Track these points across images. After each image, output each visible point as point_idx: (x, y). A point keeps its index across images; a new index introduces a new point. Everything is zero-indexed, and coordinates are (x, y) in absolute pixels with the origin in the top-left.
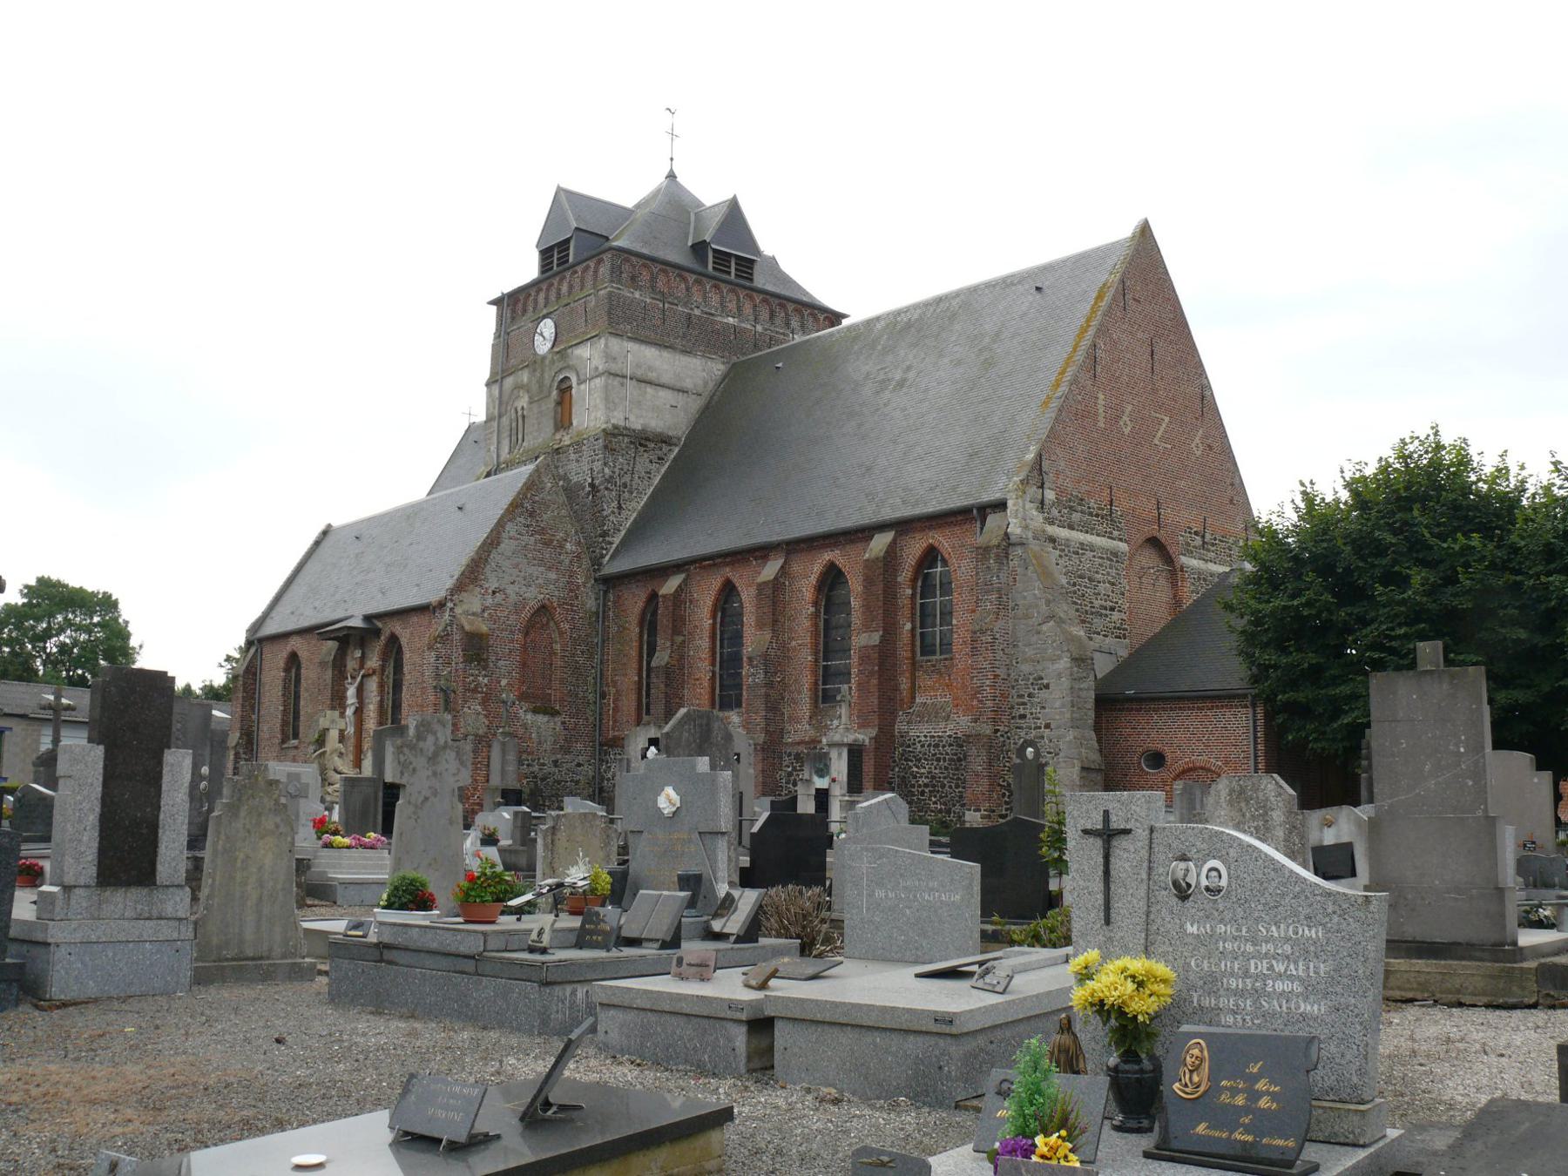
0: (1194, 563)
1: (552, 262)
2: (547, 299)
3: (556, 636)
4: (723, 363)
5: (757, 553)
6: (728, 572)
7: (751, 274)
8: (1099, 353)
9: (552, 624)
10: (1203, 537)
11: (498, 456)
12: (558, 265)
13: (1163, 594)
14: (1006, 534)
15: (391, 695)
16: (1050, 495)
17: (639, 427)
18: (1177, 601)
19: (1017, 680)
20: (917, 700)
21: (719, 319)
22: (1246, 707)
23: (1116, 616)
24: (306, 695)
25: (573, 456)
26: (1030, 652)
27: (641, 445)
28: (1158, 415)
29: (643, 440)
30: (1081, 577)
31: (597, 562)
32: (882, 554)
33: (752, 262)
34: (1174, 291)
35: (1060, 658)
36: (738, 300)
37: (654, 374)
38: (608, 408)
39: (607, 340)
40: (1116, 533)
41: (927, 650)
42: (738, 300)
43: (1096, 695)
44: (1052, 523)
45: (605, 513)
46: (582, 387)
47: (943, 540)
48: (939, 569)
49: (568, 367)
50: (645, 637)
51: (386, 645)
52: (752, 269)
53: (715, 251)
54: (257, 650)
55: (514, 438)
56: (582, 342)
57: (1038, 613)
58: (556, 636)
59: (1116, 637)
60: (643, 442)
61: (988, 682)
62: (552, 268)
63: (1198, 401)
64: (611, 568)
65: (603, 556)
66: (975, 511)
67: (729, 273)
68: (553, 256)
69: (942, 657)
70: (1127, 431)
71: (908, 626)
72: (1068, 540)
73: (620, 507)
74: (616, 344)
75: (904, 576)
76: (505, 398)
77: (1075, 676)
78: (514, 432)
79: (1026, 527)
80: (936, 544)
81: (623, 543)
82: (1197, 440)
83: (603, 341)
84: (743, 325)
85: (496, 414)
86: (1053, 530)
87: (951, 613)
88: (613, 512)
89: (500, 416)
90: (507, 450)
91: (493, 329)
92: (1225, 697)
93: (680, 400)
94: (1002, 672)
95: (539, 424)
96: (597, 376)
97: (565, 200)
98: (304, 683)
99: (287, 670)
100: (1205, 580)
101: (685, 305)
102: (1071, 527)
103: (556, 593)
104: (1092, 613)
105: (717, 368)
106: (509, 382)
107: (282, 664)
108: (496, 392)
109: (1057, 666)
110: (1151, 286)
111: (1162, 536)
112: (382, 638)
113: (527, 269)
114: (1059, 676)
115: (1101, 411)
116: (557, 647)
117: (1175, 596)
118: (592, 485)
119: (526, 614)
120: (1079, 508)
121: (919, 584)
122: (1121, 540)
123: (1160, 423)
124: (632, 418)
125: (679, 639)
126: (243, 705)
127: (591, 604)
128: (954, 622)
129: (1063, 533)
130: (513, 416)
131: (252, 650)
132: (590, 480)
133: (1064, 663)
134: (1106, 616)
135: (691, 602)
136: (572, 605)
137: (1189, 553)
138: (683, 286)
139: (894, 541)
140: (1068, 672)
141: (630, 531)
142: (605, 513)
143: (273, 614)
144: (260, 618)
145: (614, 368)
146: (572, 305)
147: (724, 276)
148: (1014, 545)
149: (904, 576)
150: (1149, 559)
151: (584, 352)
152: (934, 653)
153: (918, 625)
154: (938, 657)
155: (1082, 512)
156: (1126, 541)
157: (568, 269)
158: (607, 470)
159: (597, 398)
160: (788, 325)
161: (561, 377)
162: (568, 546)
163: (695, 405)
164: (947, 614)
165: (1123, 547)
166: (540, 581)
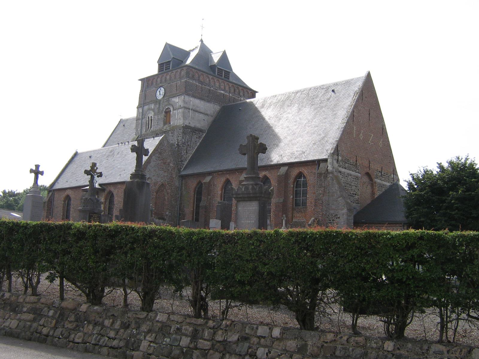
0: (378, 181)
1: (163, 68)
2: (161, 80)
3: (166, 194)
4: (219, 106)
5: (239, 171)
6: (228, 176)
7: (229, 77)
8: (355, 114)
9: (165, 190)
10: (381, 173)
11: (141, 132)
12: (165, 69)
13: (369, 190)
14: (327, 170)
15: (107, 211)
16: (340, 158)
17: (193, 126)
18: (373, 193)
19: (329, 215)
20: (294, 220)
21: (219, 91)
22: (401, 227)
23: (357, 197)
24: (73, 210)
25: (170, 134)
26: (334, 207)
27: (194, 132)
28: (370, 134)
29: (195, 130)
30: (348, 184)
31: (179, 171)
32: (284, 174)
33: (229, 72)
34: (376, 94)
35: (343, 209)
36: (225, 85)
37: (198, 109)
38: (184, 119)
39: (184, 96)
40: (357, 171)
41: (297, 204)
42: (225, 85)
43: (354, 221)
44: (340, 167)
45: (182, 154)
46: (175, 111)
47: (305, 171)
48: (302, 179)
49: (170, 104)
50: (196, 196)
51: (107, 194)
52: (229, 75)
53: (218, 68)
54: (52, 193)
55: (147, 127)
56: (175, 97)
57: (337, 195)
58: (166, 194)
59: (357, 203)
60: (195, 131)
61: (320, 216)
62: (163, 70)
63: (382, 129)
64: (183, 173)
65: (181, 169)
66: (316, 162)
67: (222, 76)
68: (164, 66)
69: (303, 207)
70: (361, 138)
71: (292, 197)
72: (344, 172)
73: (187, 152)
74: (187, 98)
75: (291, 180)
76: (144, 113)
77: (348, 215)
78: (147, 124)
79: (333, 168)
80: (302, 171)
81: (188, 164)
82: (381, 142)
83: (183, 97)
84: (226, 94)
85: (141, 117)
86: (340, 169)
87: (307, 193)
88: (185, 154)
89: (142, 119)
90: (145, 130)
91: (140, 89)
92: (394, 223)
93: (206, 118)
94: (324, 212)
95: (158, 122)
96: (180, 109)
97: (169, 49)
98: (72, 206)
99: (64, 201)
100: (381, 187)
101: (209, 86)
102: (345, 168)
103: (167, 180)
104: (350, 196)
105: (217, 108)
106: (146, 107)
107: (63, 199)
108: (141, 110)
109: (342, 212)
110: (370, 93)
111: (370, 172)
112: (106, 192)
113: (153, 70)
114: (343, 214)
115: (355, 132)
116: (166, 198)
117: (373, 191)
118: (178, 145)
119: (157, 187)
120: (348, 162)
121: (295, 183)
122: (358, 173)
123: (371, 136)
124: (191, 123)
125: (209, 197)
126: (47, 213)
127: (177, 184)
128: (308, 196)
129: (343, 170)
130: (147, 119)
131: (51, 194)
132: (177, 143)
133: (345, 211)
134: (354, 196)
135: (214, 185)
136: (171, 184)
137: (377, 178)
138: (208, 79)
139: (288, 170)
140: (346, 214)
141: (189, 161)
142: (182, 154)
143: (59, 181)
144: (52, 183)
145: (186, 105)
146: (171, 84)
147: (221, 77)
148: (329, 173)
149: (291, 180)
150: (366, 179)
151: (176, 100)
152: (300, 206)
153: (295, 197)
154: (301, 207)
155: (348, 164)
156: (360, 173)
157: (170, 71)
158: (183, 140)
159: (180, 115)
160: (239, 94)
161: (167, 107)
162: (171, 164)
163: (211, 119)
164: (305, 193)
165: (359, 175)
166: (162, 176)
